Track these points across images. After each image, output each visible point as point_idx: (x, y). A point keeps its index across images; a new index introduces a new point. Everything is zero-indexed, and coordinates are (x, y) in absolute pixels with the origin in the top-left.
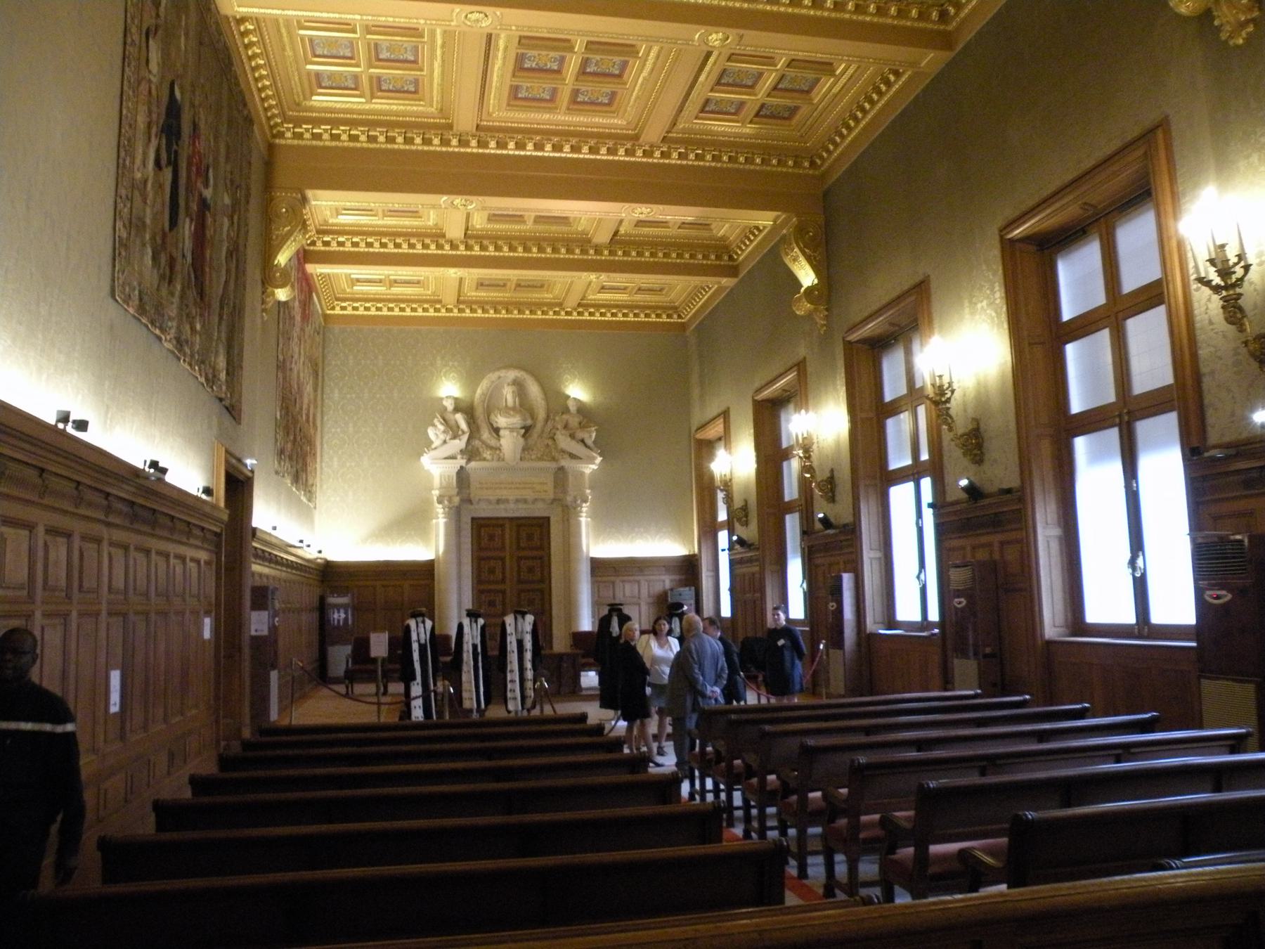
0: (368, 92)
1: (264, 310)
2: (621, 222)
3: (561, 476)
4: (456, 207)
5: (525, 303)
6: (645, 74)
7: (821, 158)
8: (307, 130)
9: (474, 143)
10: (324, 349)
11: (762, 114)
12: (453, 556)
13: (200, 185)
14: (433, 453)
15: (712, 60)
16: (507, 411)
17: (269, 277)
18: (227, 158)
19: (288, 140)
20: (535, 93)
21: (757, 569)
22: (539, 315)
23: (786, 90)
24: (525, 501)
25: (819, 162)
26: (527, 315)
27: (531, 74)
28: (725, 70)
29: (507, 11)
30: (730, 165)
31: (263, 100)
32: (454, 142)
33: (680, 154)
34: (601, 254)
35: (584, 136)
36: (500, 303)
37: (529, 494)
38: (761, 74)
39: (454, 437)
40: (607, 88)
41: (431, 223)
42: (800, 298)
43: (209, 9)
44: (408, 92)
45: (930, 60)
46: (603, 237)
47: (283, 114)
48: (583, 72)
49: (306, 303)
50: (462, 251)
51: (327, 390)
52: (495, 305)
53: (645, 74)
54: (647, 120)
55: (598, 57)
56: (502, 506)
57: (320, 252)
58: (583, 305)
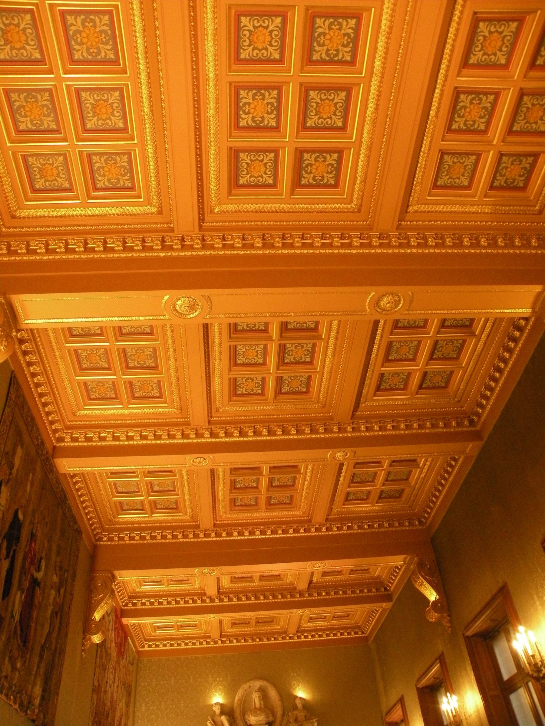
0: (149, 511)
1: (83, 651)
2: (313, 573)
4: (204, 575)
5: (263, 634)
6: (307, 482)
7: (425, 518)
8: (116, 535)
9: (213, 535)
10: (137, 674)
11: (382, 496)
13: (32, 570)
15: (344, 469)
17: (88, 626)
18: (58, 554)
19: (105, 542)
20: (246, 502)
22: (273, 641)
23: (394, 480)
25: (424, 520)
26: (265, 641)
27: (242, 491)
28: (354, 474)
29: (215, 455)
30: (370, 530)
31: (89, 520)
32: (202, 535)
33: (338, 527)
34: (304, 597)
35: (279, 524)
36: (248, 635)
38: (376, 473)
40: (287, 494)
41: (197, 586)
42: (429, 610)
43: (52, 471)
44: (172, 508)
45: (471, 448)
46: (303, 585)
47: (102, 527)
48: (270, 485)
49: (122, 646)
50: (217, 603)
51: (138, 705)
52: (244, 637)
53: (307, 482)
54: (313, 510)
55: (278, 476)
57: (131, 610)
58: (299, 631)
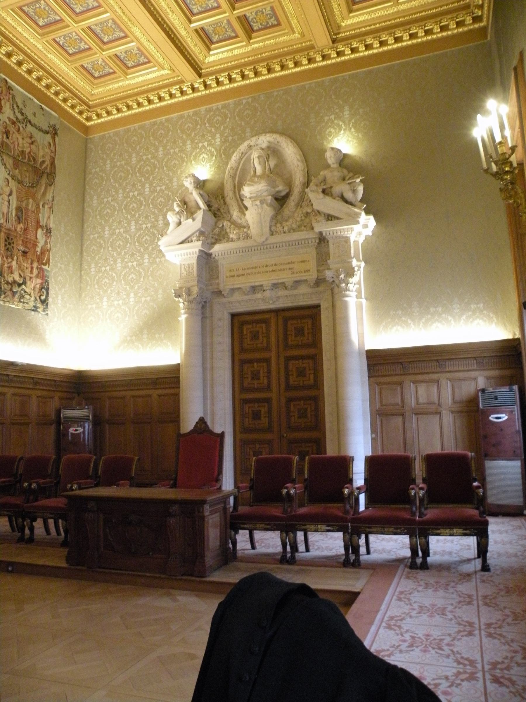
12: (197, 360)
21: (240, 508)
24: (283, 285)
37: (287, 277)
56: (259, 296)
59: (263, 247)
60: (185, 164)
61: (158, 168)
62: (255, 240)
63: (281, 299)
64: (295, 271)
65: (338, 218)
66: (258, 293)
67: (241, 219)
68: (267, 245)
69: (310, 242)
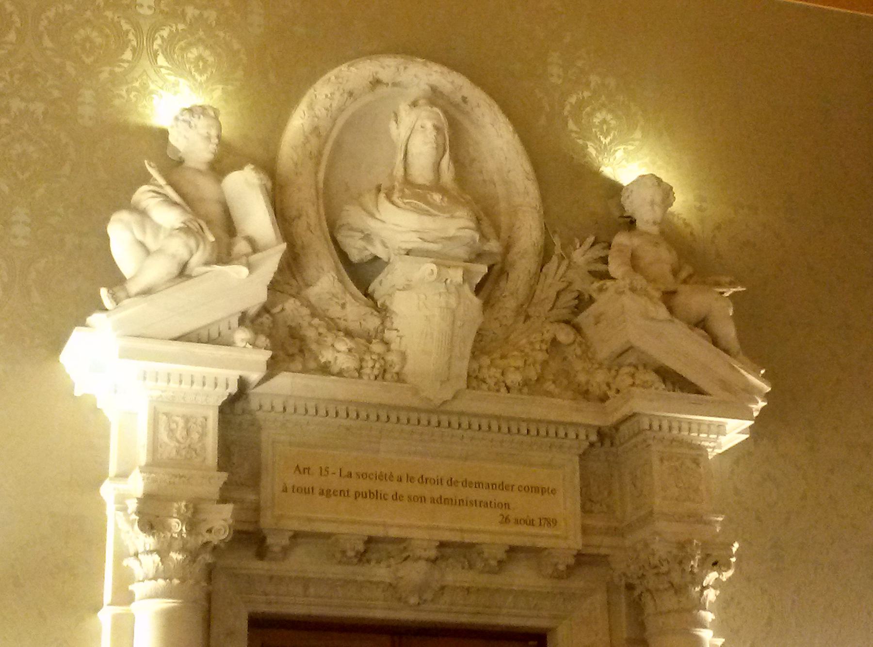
3: (608, 454)
14: (133, 310)
16: (412, 191)
37: (484, 528)
39: (223, 256)
56: (381, 572)
59: (433, 417)
60: (128, 55)
61: (18, 32)
62: (416, 391)
63: (446, 598)
64: (512, 514)
65: (700, 392)
66: (379, 562)
67: (343, 306)
68: (450, 413)
69: (572, 435)
